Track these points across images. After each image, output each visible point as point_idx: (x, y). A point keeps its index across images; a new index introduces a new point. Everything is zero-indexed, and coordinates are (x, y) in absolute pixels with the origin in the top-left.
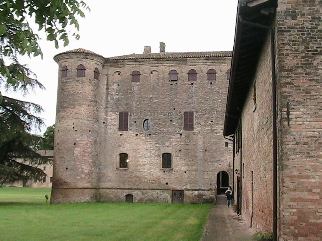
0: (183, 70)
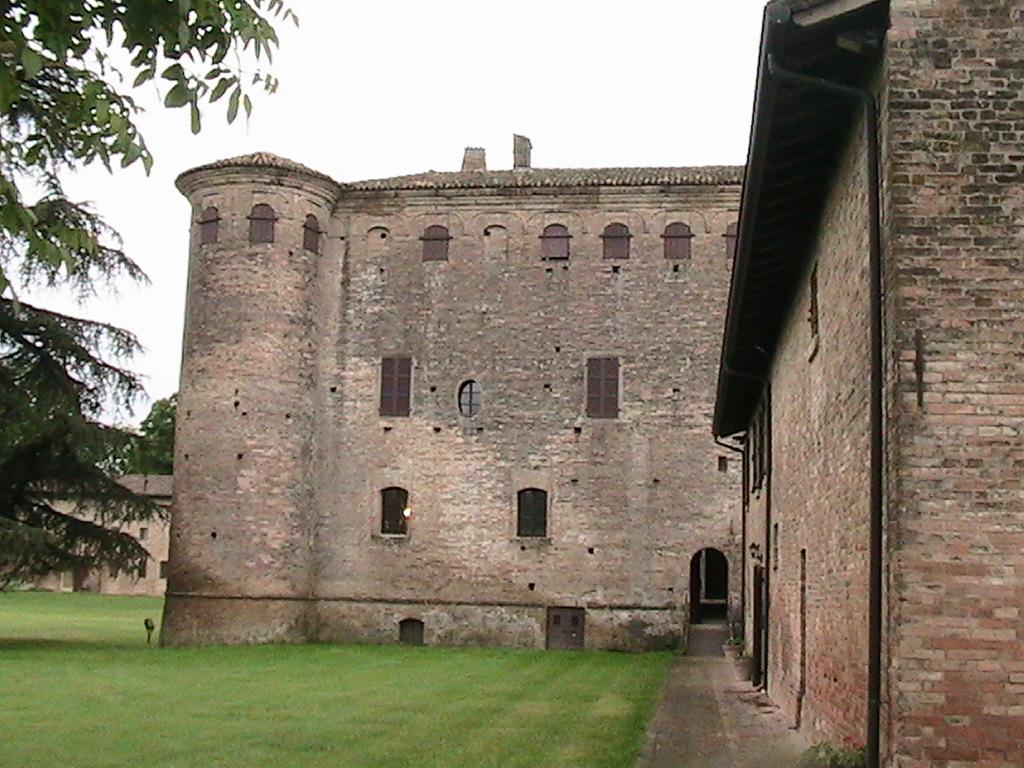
0: (587, 225)
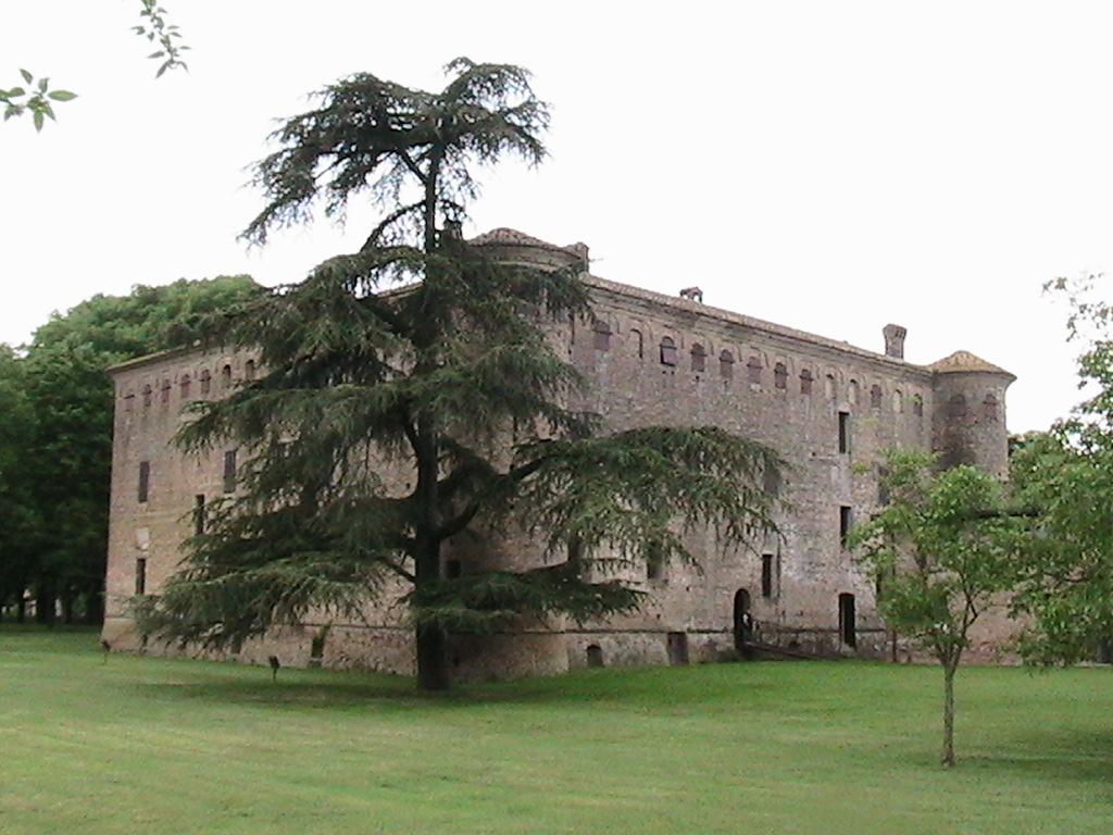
0: (796, 362)
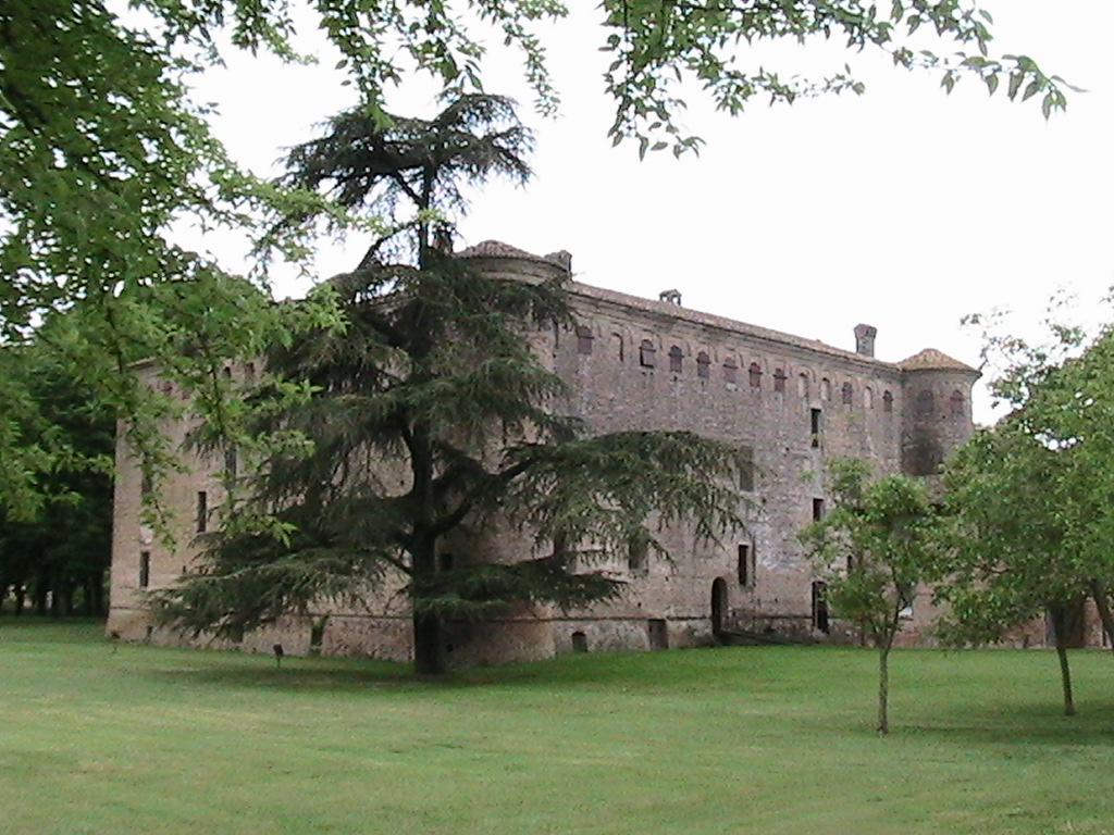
0: (770, 363)
